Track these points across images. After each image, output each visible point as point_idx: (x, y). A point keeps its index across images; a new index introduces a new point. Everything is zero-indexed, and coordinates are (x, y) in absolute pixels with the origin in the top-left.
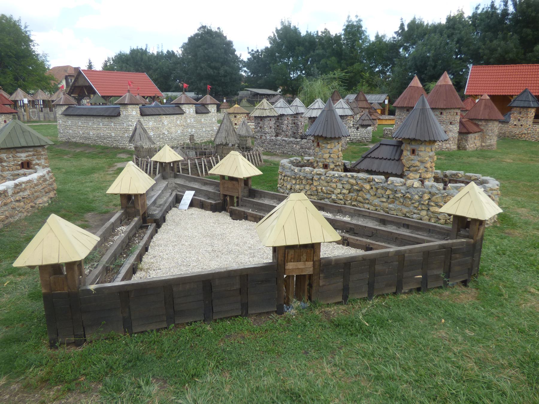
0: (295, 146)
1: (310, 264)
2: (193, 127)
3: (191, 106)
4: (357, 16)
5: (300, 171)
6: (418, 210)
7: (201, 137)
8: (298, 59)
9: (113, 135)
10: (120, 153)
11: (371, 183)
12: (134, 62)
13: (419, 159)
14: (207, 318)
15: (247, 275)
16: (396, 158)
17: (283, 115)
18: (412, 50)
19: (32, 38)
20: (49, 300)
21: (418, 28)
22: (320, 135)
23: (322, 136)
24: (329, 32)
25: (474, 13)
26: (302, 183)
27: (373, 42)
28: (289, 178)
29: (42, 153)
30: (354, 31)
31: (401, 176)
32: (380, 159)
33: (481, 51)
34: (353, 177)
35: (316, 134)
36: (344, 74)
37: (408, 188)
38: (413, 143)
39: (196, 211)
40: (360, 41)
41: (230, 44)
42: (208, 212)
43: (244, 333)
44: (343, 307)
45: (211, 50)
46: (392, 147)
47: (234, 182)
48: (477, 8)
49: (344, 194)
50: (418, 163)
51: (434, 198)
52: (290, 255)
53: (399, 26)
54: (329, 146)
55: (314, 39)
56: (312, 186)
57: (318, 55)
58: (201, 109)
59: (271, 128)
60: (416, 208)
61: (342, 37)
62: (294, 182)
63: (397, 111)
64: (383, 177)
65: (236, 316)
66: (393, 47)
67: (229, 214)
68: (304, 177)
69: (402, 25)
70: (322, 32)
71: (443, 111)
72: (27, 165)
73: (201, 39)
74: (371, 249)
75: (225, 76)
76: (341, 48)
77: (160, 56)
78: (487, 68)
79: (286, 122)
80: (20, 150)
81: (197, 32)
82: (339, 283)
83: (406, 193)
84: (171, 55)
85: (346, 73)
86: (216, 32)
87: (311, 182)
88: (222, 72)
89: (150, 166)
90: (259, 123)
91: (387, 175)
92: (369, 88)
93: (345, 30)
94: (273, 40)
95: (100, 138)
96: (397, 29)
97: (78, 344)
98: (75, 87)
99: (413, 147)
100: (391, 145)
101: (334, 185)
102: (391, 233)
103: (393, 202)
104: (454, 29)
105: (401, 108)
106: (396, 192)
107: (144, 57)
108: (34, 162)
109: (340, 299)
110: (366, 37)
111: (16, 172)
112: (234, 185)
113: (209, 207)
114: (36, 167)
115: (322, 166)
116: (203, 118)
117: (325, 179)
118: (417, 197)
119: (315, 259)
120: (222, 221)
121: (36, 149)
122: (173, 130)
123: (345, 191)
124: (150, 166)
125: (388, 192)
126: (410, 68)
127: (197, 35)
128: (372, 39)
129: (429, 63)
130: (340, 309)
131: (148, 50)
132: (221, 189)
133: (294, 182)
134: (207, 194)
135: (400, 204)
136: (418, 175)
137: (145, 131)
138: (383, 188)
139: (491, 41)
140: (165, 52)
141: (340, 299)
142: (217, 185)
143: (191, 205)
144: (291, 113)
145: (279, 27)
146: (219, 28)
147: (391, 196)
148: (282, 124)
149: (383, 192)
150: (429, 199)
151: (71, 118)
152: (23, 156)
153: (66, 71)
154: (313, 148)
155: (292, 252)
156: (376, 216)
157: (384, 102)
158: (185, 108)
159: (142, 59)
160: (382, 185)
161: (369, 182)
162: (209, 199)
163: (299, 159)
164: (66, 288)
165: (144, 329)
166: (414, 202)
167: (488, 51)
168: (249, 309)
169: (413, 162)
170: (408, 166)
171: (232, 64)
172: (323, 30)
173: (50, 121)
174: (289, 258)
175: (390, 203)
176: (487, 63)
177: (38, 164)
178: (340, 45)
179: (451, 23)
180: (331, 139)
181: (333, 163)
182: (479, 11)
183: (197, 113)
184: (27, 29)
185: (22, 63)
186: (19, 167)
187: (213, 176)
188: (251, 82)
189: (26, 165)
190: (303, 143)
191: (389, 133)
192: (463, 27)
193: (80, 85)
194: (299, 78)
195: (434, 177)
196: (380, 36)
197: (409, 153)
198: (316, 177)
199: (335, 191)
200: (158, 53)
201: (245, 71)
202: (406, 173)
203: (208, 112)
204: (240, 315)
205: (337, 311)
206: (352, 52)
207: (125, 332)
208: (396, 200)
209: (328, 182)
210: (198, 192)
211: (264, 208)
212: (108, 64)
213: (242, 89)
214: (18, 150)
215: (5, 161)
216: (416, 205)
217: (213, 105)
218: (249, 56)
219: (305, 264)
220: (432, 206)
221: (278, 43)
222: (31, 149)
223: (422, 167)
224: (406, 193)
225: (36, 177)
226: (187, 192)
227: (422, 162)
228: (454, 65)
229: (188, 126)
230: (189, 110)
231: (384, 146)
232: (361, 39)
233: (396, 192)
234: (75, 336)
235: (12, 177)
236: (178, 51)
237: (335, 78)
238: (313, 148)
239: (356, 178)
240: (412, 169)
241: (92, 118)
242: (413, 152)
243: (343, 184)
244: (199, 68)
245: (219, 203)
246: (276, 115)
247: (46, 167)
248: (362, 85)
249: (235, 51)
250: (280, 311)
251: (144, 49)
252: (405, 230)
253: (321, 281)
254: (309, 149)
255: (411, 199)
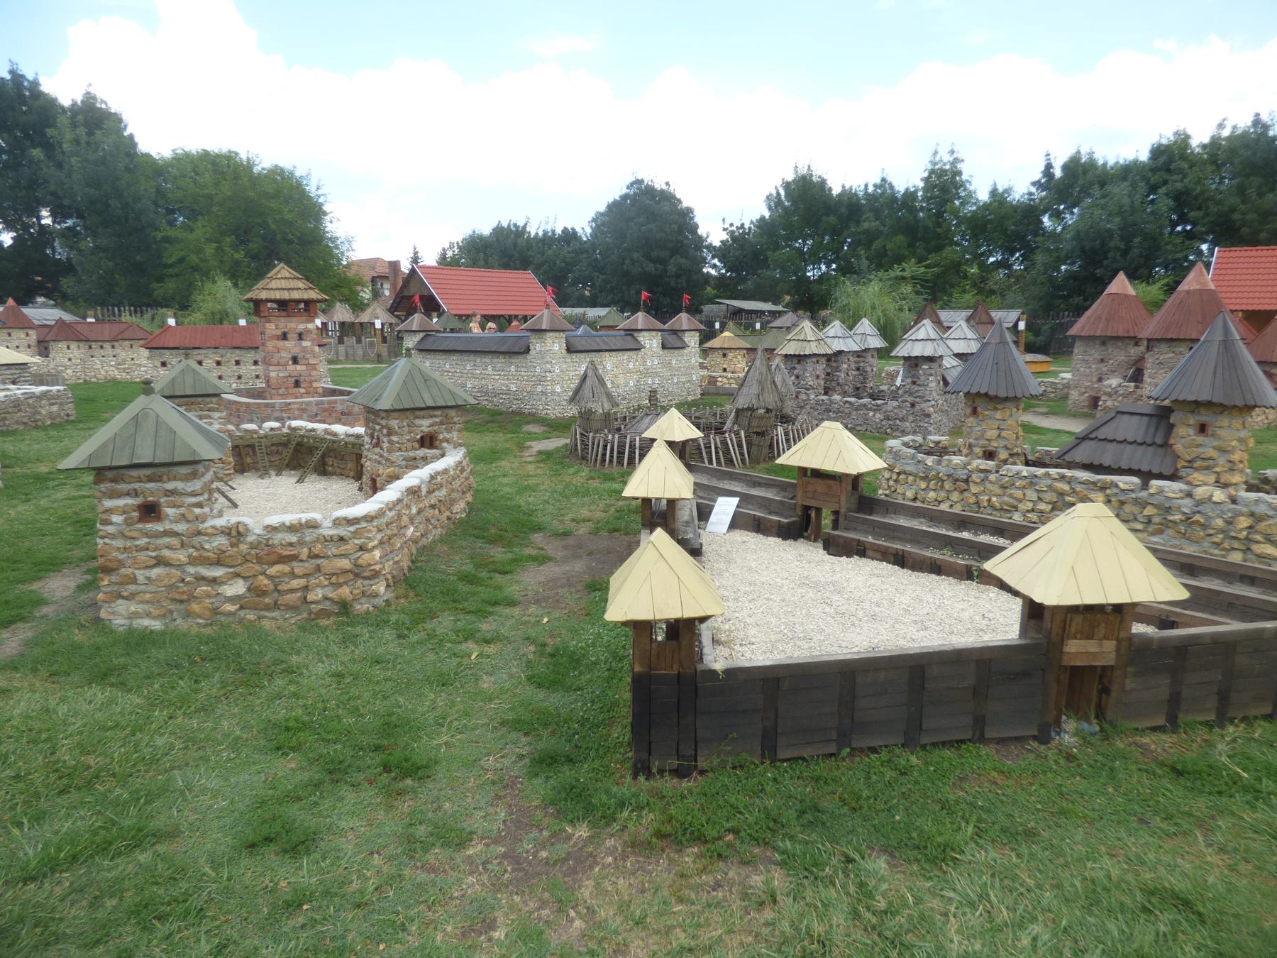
0: (871, 414)
1: (1110, 645)
2: (656, 374)
3: (654, 333)
4: (952, 152)
5: (939, 463)
6: (1224, 549)
7: (671, 394)
8: (828, 242)
9: (513, 388)
10: (529, 423)
11: (1108, 491)
12: (502, 250)
13: (1216, 443)
14: (910, 741)
15: (991, 660)
16: (1159, 440)
17: (840, 352)
18: (1069, 219)
19: (325, 208)
20: (642, 685)
21: (1085, 173)
22: (983, 391)
23: (986, 394)
24: (892, 187)
25: (1213, 137)
26: (942, 487)
27: (985, 204)
28: (911, 478)
29: (456, 419)
30: (945, 183)
31: (1173, 477)
32: (1120, 442)
33: (1236, 216)
34: (1063, 477)
35: (974, 391)
36: (923, 269)
37: (1200, 503)
38: (1203, 411)
39: (740, 536)
40: (957, 202)
41: (688, 213)
42: (771, 539)
43: (989, 775)
44: (1167, 739)
45: (652, 226)
46: (1146, 419)
47: (832, 482)
48: (1221, 126)
49: (1041, 512)
50: (1212, 453)
51: (1262, 526)
52: (1074, 624)
53: (1043, 168)
54: (998, 415)
55: (858, 199)
56: (967, 494)
57: (866, 232)
58: (672, 340)
59: (818, 377)
60: (1217, 545)
61: (920, 194)
62: (923, 485)
63: (1077, 344)
64: (1136, 480)
65: (963, 741)
66: (1029, 213)
67: (820, 545)
68: (949, 476)
69: (1049, 166)
70: (875, 186)
71: (116, 344)
72: (428, 441)
73: (632, 205)
74: (1172, 625)
75: (678, 276)
76: (915, 217)
77: (548, 240)
78: (1254, 253)
79: (845, 366)
80: (421, 413)
81: (625, 191)
82: (1161, 687)
83: (1194, 513)
84: (570, 236)
85: (927, 267)
86: (662, 191)
87: (964, 486)
88: (672, 268)
89: (612, 449)
90: (794, 368)
91: (1146, 476)
92: (978, 297)
93: (926, 180)
94: (774, 202)
95: (486, 393)
96: (1037, 175)
97: (680, 773)
98: (403, 298)
99: (1203, 419)
100: (1142, 415)
101: (1019, 494)
102: (1218, 593)
103: (1160, 532)
104: (1168, 171)
105: (1090, 339)
106: (1168, 510)
107: (519, 241)
108: (441, 437)
109: (1161, 721)
110: (970, 194)
111: (412, 454)
112: (829, 487)
113: (774, 530)
114: (444, 444)
115: (981, 454)
116: (674, 359)
117: (998, 480)
118: (1219, 522)
119: (1123, 635)
120: (805, 559)
121: (446, 411)
122: (621, 381)
123: (1042, 506)
124: (612, 449)
125: (1149, 511)
126: (1067, 257)
127: (624, 197)
128: (983, 196)
129: (1112, 244)
130: (1165, 742)
131: (528, 229)
132: (799, 495)
133: (923, 485)
134: (765, 504)
135: (1178, 535)
136: (1212, 479)
137: (602, 382)
138: (1137, 502)
139: (1261, 195)
140: (559, 231)
141: (1161, 721)
142: (782, 487)
143: (735, 524)
144: (856, 348)
145: (790, 177)
146: (667, 184)
147: (1156, 520)
148: (837, 369)
149: (1136, 509)
150: (1250, 527)
151: (431, 356)
152: (425, 425)
153: (373, 268)
154: (911, 418)
155: (1078, 619)
156: (1173, 557)
157: (1016, 325)
158: (644, 338)
159: (515, 245)
160: (1133, 495)
161: (1103, 489)
162: (770, 513)
163: (919, 439)
164: (676, 666)
165: (795, 754)
166: (1212, 532)
167: (1255, 216)
168: (987, 729)
169: (1201, 450)
170: (1189, 458)
171: (692, 251)
172: (878, 181)
173: (355, 362)
174: (1073, 630)
175: (1153, 534)
176: (1253, 241)
177: (447, 441)
178: (913, 210)
179: (1162, 159)
180: (1006, 399)
181: (1006, 448)
182: (1226, 133)
183: (664, 347)
184: (320, 192)
185: (310, 254)
186: (417, 445)
187: (785, 469)
188: (726, 287)
189: (427, 442)
190: (889, 408)
191: (1050, 389)
192: (1191, 167)
193: (411, 294)
194: (822, 279)
195: (1246, 482)
196: (1001, 190)
197: (1191, 432)
198: (975, 477)
199: (1021, 506)
200: (545, 233)
201: (714, 266)
202: (1182, 473)
203: (683, 346)
204: (1035, 738)
205: (1163, 744)
206: (939, 225)
207: (763, 756)
208: (1168, 527)
209: (1004, 487)
210: (745, 499)
211: (901, 535)
212: (449, 254)
213: (711, 301)
214: (418, 413)
215: (396, 433)
216: (1216, 540)
217: (692, 333)
218: (725, 236)
219: (1101, 645)
220: (1258, 542)
221: (785, 209)
222: (438, 413)
223: (1222, 461)
224: (1194, 513)
225: (452, 464)
226: (721, 500)
227: (1223, 451)
228: (1169, 247)
229: (647, 373)
230: (651, 342)
231: (1126, 417)
232: (959, 198)
233: (1168, 510)
234: (679, 757)
235: (404, 463)
236: (584, 228)
237: (903, 278)
238: (911, 418)
239: (1069, 481)
240: (1198, 464)
241: (472, 357)
242: (1202, 429)
243: (1038, 491)
244: (627, 261)
245: (794, 523)
246: (830, 352)
247: (460, 445)
248: (964, 291)
249: (696, 226)
250: (1044, 739)
251: (521, 224)
252: (1248, 588)
253: (1127, 681)
254: (902, 420)
255: (1204, 526)
